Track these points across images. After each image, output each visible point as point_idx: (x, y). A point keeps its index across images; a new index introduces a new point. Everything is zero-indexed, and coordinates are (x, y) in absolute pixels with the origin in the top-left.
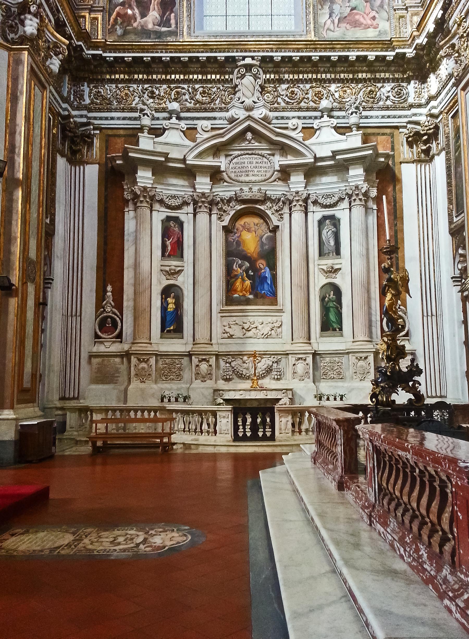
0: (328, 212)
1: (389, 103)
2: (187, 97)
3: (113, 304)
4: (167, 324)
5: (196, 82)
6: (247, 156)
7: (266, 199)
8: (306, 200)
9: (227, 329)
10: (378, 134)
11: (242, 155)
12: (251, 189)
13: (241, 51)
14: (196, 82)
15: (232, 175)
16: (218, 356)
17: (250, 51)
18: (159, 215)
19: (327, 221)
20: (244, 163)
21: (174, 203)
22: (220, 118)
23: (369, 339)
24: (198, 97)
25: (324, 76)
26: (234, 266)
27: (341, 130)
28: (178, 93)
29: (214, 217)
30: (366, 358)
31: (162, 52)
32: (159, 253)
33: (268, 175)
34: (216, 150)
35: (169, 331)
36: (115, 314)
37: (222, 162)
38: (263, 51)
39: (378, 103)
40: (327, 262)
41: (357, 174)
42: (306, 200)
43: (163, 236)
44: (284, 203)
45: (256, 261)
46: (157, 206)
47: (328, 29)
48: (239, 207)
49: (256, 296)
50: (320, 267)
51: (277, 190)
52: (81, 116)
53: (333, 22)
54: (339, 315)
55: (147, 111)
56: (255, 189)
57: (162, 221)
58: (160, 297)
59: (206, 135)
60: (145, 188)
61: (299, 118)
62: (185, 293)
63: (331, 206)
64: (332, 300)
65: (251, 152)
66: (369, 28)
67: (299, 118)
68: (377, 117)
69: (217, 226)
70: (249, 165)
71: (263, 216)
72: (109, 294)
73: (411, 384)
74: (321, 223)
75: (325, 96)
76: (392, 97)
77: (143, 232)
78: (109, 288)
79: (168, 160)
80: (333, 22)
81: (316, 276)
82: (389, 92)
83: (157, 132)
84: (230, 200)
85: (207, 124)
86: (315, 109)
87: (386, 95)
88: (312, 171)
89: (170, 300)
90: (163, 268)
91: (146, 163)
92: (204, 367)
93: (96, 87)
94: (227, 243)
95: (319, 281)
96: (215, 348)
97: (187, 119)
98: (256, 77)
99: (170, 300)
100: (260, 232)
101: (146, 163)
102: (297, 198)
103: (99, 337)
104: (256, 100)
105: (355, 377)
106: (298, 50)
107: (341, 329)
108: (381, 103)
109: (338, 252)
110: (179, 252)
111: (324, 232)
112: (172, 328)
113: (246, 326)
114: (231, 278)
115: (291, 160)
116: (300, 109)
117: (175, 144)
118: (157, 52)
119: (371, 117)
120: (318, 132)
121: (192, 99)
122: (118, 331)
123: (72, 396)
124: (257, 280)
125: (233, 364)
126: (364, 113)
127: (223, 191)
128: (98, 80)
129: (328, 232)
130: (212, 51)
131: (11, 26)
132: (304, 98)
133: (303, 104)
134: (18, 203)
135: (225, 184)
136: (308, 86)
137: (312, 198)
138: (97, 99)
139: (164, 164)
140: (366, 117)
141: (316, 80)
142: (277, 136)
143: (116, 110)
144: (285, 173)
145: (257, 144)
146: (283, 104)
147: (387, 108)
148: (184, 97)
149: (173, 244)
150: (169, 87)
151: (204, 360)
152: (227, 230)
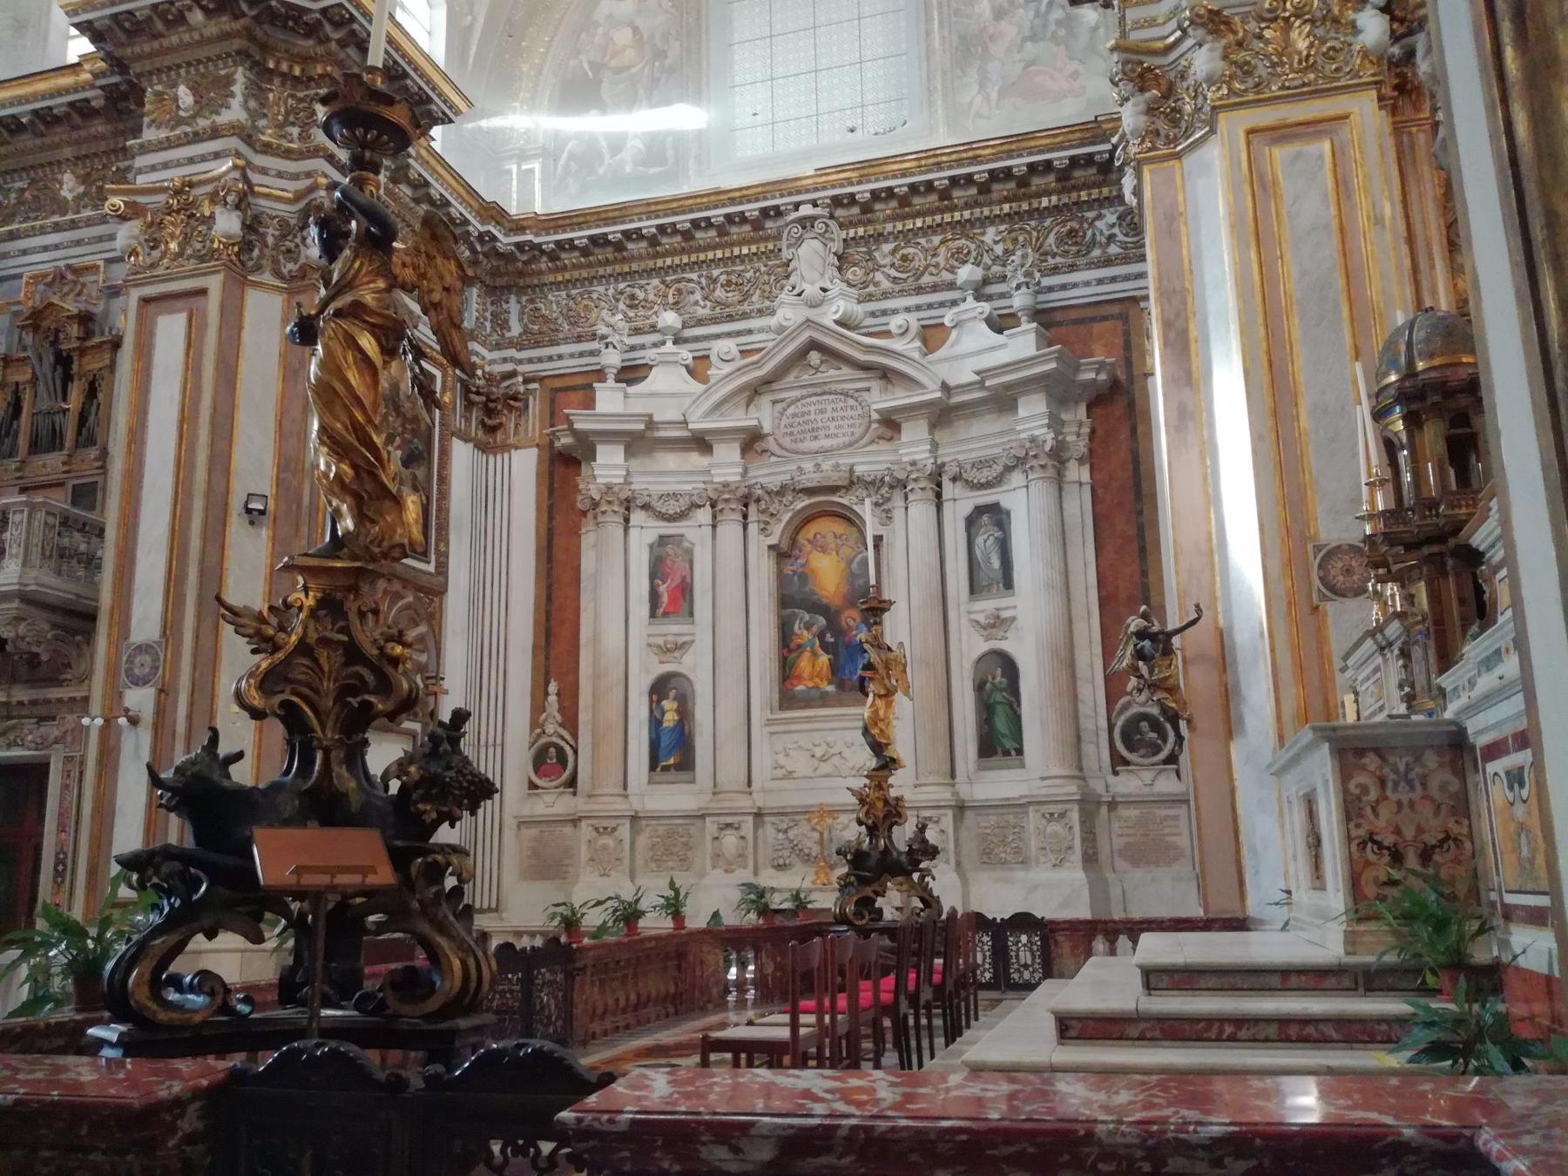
0: (986, 497)
1: (1114, 249)
2: (698, 296)
3: (559, 718)
4: (662, 753)
5: (715, 262)
6: (814, 399)
7: (852, 483)
8: (936, 478)
9: (782, 760)
10: (1093, 319)
11: (803, 397)
12: (818, 465)
13: (790, 194)
14: (715, 262)
15: (786, 441)
16: (759, 815)
17: (808, 191)
18: (645, 531)
19: (985, 518)
20: (809, 413)
21: (672, 508)
22: (761, 330)
23: (1077, 773)
24: (719, 293)
25: (967, 214)
26: (796, 627)
27: (999, 324)
28: (679, 291)
29: (753, 528)
30: (1063, 815)
31: (640, 220)
32: (645, 610)
33: (858, 431)
34: (754, 391)
35: (666, 769)
36: (563, 738)
37: (763, 415)
38: (833, 187)
39: (1089, 252)
40: (986, 606)
41: (1032, 414)
42: (936, 478)
43: (652, 577)
44: (892, 487)
45: (838, 613)
46: (637, 517)
47: (979, 115)
48: (799, 505)
49: (841, 686)
50: (974, 616)
51: (870, 462)
52: (505, 360)
53: (987, 98)
54: (1016, 719)
55: (614, 339)
56: (827, 465)
57: (651, 546)
58: (646, 699)
59: (727, 368)
60: (609, 487)
61: (908, 310)
62: (698, 688)
63: (987, 485)
64: (999, 685)
65: (822, 390)
66: (1065, 96)
67: (908, 310)
68: (1087, 284)
69: (759, 544)
70: (819, 417)
71: (850, 519)
72: (553, 698)
73: (916, 876)
74: (971, 522)
75: (974, 254)
76: (1121, 237)
77: (615, 568)
78: (553, 687)
79: (651, 423)
80: (987, 98)
81: (964, 637)
82: (1113, 225)
83: (631, 374)
84: (782, 491)
85: (728, 346)
86: (951, 286)
87: (1107, 233)
88: (943, 414)
89: (666, 704)
90: (653, 640)
91: (611, 436)
92: (730, 840)
93: (532, 301)
94: (782, 580)
95: (970, 647)
96: (760, 801)
97: (697, 339)
98: (824, 237)
99: (666, 704)
100: (846, 551)
101: (611, 436)
102: (914, 476)
103: (537, 787)
104: (827, 285)
105: (1042, 859)
106: (904, 173)
107: (1020, 752)
108: (1096, 253)
109: (1008, 583)
110: (685, 606)
111: (979, 540)
112: (672, 761)
113: (819, 752)
114: (790, 651)
115: (900, 398)
116: (920, 290)
117: (669, 392)
118: (632, 221)
119: (1075, 285)
120: (954, 333)
121: (706, 298)
122: (568, 772)
123: (485, 905)
124: (842, 650)
125: (791, 834)
126: (1046, 282)
127: (769, 474)
128: (533, 287)
129: (986, 541)
130: (733, 202)
131: (289, 251)
132: (927, 267)
133: (926, 279)
134: (1152, 355)
135: (773, 459)
136: (936, 240)
137: (951, 470)
138: (533, 323)
139: (648, 434)
140: (1050, 289)
141: (953, 225)
142: (866, 352)
143: (566, 340)
144: (890, 424)
145: (832, 372)
146: (886, 284)
147: (1108, 262)
148: (692, 298)
149: (671, 594)
150: (663, 282)
151: (729, 825)
152: (781, 554)
